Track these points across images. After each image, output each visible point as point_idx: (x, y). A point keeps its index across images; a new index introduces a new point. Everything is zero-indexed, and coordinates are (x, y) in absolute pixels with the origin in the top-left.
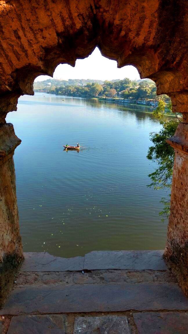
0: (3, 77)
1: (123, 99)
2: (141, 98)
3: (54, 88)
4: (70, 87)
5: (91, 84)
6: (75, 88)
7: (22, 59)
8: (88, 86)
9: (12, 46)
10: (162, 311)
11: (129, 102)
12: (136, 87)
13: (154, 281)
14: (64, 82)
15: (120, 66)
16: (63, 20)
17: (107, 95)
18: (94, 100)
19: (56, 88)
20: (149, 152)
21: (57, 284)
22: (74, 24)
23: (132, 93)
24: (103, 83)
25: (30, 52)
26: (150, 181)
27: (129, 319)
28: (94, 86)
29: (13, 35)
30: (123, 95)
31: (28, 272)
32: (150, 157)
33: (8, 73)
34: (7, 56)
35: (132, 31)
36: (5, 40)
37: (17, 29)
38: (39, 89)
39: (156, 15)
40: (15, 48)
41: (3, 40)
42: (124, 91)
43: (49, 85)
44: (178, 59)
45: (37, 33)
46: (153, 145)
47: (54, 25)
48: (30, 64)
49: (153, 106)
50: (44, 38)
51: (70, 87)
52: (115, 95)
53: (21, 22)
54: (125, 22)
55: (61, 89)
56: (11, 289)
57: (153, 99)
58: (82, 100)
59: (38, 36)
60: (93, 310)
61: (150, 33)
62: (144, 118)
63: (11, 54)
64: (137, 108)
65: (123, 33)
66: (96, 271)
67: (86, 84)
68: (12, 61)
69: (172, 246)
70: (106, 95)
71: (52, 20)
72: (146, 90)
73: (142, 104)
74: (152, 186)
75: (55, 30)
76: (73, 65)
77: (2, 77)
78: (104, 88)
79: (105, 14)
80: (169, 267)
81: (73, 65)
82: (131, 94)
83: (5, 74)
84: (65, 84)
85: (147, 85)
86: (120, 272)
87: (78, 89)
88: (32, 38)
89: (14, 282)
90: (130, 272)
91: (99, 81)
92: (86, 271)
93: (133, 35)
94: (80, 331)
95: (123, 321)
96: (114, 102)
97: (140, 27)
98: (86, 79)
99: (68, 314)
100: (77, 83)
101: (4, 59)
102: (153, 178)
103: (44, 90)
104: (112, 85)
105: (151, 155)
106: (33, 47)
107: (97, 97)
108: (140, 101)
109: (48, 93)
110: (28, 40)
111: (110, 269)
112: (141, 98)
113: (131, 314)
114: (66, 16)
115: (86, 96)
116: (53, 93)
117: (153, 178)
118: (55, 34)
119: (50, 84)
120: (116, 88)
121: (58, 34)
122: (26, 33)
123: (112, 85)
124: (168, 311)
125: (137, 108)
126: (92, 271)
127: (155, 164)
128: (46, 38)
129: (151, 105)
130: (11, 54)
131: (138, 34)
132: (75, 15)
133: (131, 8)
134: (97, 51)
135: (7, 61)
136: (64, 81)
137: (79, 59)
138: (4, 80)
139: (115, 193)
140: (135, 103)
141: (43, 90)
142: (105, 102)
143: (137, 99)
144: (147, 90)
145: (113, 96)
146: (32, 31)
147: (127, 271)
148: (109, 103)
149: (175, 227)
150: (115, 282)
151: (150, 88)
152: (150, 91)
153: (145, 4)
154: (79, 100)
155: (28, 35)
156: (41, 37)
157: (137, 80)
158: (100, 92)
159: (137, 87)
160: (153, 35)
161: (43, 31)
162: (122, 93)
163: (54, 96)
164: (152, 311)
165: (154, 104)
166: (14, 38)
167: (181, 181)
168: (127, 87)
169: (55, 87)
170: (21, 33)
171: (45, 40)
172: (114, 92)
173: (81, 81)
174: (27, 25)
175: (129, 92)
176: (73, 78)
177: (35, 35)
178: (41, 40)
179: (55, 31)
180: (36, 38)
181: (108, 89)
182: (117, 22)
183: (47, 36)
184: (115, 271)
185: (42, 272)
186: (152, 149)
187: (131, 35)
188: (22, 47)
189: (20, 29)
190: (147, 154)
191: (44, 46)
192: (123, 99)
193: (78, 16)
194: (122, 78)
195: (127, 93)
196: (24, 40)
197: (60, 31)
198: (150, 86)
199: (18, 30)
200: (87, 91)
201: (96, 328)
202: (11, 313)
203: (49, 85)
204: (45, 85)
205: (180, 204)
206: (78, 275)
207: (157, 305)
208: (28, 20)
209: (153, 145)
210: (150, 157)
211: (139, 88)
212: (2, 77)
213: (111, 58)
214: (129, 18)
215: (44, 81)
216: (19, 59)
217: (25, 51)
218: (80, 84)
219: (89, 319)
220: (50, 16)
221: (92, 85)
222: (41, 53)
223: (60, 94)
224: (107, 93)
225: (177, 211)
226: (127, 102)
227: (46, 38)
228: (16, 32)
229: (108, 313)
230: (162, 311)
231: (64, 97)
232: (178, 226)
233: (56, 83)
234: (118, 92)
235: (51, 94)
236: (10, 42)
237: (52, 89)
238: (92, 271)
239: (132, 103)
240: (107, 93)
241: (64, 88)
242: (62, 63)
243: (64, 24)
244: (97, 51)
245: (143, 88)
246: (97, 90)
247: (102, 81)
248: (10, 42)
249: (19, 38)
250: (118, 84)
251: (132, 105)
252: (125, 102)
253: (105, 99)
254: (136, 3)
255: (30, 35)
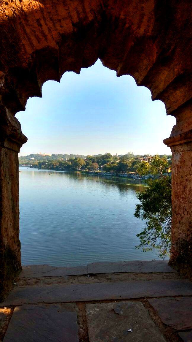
0: (25, 56)
1: (105, 172)
2: (123, 171)
3: (37, 162)
4: (54, 161)
5: (74, 158)
6: (58, 163)
7: (42, 42)
8: (71, 160)
9: (34, 31)
10: (178, 296)
11: (111, 175)
12: (117, 161)
13: (164, 279)
14: (47, 157)
15: (119, 75)
16: (78, 13)
17: (89, 169)
18: (77, 173)
19: (39, 163)
20: (136, 209)
21: (61, 284)
22: (86, 17)
23: (114, 166)
24: (85, 158)
25: (49, 37)
26: (138, 241)
27: (144, 303)
28: (77, 160)
29: (36, 23)
30: (105, 169)
31: (27, 277)
32: (137, 215)
33: (29, 53)
34: (29, 39)
35: (134, 24)
36: (29, 27)
37: (40, 18)
38: (22, 163)
39: (153, 13)
40: (37, 33)
41: (27, 26)
42: (105, 164)
43: (31, 159)
44: (172, 47)
45: (56, 23)
46: (139, 202)
47: (70, 17)
48: (48, 46)
49: (135, 178)
50: (61, 27)
51: (54, 161)
52: (97, 168)
53: (43, 13)
54: (129, 17)
55: (44, 163)
56: (10, 289)
57: (134, 172)
58: (65, 173)
59: (57, 25)
60: (103, 299)
61: (148, 26)
62: (126, 190)
63: (33, 38)
64: (119, 181)
65: (127, 26)
66: (102, 274)
67: (69, 159)
68: (33, 43)
69: (178, 246)
70: (88, 168)
71: (69, 13)
72: (126, 163)
73: (124, 177)
74: (142, 247)
75: (71, 21)
76: (78, 72)
77: (24, 56)
78: (86, 162)
79: (112, 10)
80: (177, 269)
81: (78, 72)
82: (112, 167)
83: (26, 54)
84: (48, 158)
85: (127, 159)
86: (126, 274)
87: (61, 163)
88: (52, 26)
89: (13, 285)
90: (137, 274)
91: (82, 156)
92: (92, 275)
93: (135, 27)
94: (93, 313)
95: (139, 305)
96: (96, 175)
97: (141, 21)
98: (69, 154)
99: (77, 303)
100: (60, 158)
101: (27, 41)
102: (141, 238)
103: (27, 165)
104: (94, 160)
105: (139, 213)
106: (52, 33)
107: (79, 171)
108: (122, 173)
109: (31, 167)
110: (48, 28)
111: (116, 273)
112: (123, 171)
113: (145, 300)
114: (81, 10)
115: (69, 170)
116: (35, 168)
117: (141, 238)
118: (71, 25)
119: (33, 158)
120: (98, 162)
121: (74, 25)
122: (47, 22)
123: (94, 160)
124: (184, 296)
125: (119, 181)
126: (97, 275)
127: (142, 224)
128: (63, 26)
129: (132, 178)
130: (33, 38)
131: (139, 27)
132: (88, 10)
133: (133, 7)
134: (99, 62)
135: (29, 43)
136: (47, 156)
137: (83, 68)
138: (25, 58)
139: (106, 252)
140: (117, 176)
141: (26, 164)
142: (88, 175)
143: (119, 172)
144: (128, 164)
145: (95, 170)
146: (52, 21)
147: (134, 273)
148: (92, 176)
149: (179, 224)
150: (123, 280)
151: (130, 162)
152: (131, 164)
153: (143, 5)
154: (61, 173)
155: (48, 23)
156: (59, 26)
157: (117, 155)
158: (83, 166)
159: (118, 161)
160: (151, 28)
161: (62, 21)
162: (104, 166)
163: (37, 170)
164: (167, 297)
165: (135, 177)
166: (36, 25)
167: (180, 175)
168: (108, 161)
169: (38, 162)
170: (42, 22)
171: (62, 28)
172: (96, 166)
173: (64, 156)
174: (48, 16)
175: (110, 166)
176: (56, 153)
177: (54, 25)
178: (58, 28)
179: (71, 22)
180: (55, 27)
181: (90, 163)
182: (122, 17)
183: (65, 25)
184: (122, 274)
185: (43, 277)
186: (138, 207)
187: (134, 27)
188: (43, 32)
189: (42, 19)
190: (134, 211)
191: (61, 32)
192: (105, 172)
193: (90, 11)
194: (103, 153)
195: (109, 166)
196: (45, 28)
197: (75, 22)
198: (130, 160)
199: (40, 19)
200: (70, 165)
201: (110, 310)
202: (14, 304)
203: (32, 160)
204: (28, 159)
205: (182, 198)
206: (83, 278)
207: (170, 293)
208: (49, 13)
209: (139, 202)
210: (137, 215)
211: (120, 162)
212: (24, 56)
213: (112, 68)
214: (132, 14)
215: (28, 156)
216: (39, 42)
217: (45, 36)
218: (63, 159)
219: (101, 305)
220: (68, 10)
221: (75, 160)
222: (59, 39)
223: (43, 168)
224: (89, 166)
225: (180, 207)
226: (109, 175)
227: (63, 26)
228: (38, 21)
229: (121, 300)
230: (178, 296)
231: (47, 171)
232: (182, 221)
233: (39, 158)
234: (100, 166)
235: (34, 168)
236: (33, 28)
237: (35, 164)
238: (97, 275)
239: (114, 176)
240: (89, 166)
241: (47, 162)
242: (69, 71)
243: (78, 16)
244: (99, 62)
245: (124, 161)
246: (79, 164)
247: (84, 156)
248: (33, 28)
249: (40, 25)
250: (100, 159)
251: (114, 177)
252: (107, 175)
253: (88, 172)
254: (136, 4)
255: (50, 24)
